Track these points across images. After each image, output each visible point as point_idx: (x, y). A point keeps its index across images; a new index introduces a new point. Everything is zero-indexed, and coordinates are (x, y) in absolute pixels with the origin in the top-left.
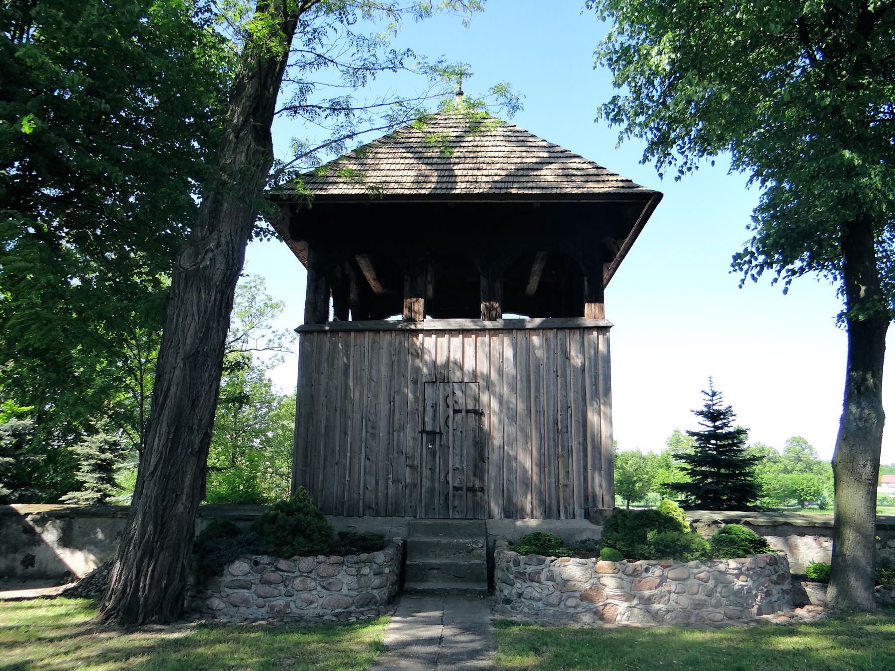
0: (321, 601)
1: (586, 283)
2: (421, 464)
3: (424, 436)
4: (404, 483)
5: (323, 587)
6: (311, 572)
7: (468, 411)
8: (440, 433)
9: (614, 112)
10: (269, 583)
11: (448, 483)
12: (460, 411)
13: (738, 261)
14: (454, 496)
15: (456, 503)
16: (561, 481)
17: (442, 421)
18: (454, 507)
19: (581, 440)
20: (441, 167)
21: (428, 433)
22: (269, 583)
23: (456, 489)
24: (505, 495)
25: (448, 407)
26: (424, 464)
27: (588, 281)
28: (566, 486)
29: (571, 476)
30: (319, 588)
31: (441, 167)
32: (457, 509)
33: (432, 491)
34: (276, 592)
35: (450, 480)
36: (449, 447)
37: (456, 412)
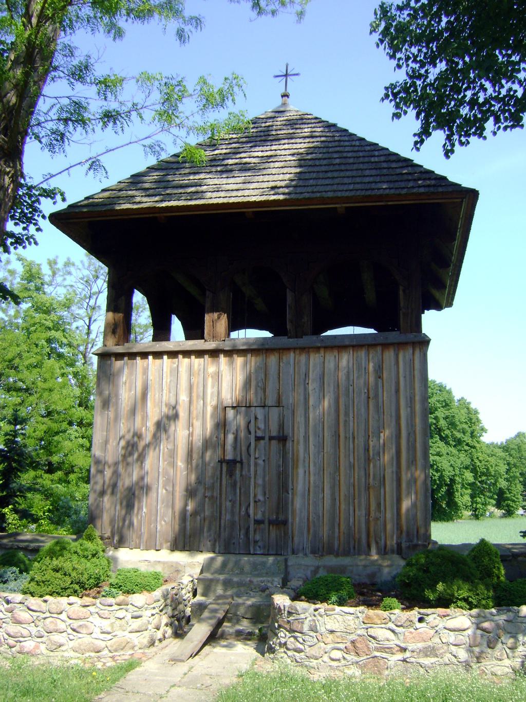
0: (71, 644)
1: (401, 293)
2: (221, 494)
3: (224, 466)
4: (202, 515)
5: (74, 630)
6: (61, 613)
7: (271, 438)
8: (241, 462)
9: (401, 96)
10: (18, 622)
11: (249, 516)
12: (263, 438)
13: (57, 257)
14: (255, 531)
15: (258, 537)
16: (372, 514)
17: (244, 448)
18: (256, 542)
19: (395, 469)
20: (391, 178)
21: (228, 462)
22: (18, 622)
23: (258, 522)
24: (311, 531)
25: (250, 433)
26: (223, 496)
27: (404, 291)
28: (377, 519)
29: (382, 508)
30: (70, 631)
31: (391, 178)
32: (260, 544)
33: (233, 524)
34: (25, 632)
35: (251, 512)
36: (250, 478)
37: (258, 439)
